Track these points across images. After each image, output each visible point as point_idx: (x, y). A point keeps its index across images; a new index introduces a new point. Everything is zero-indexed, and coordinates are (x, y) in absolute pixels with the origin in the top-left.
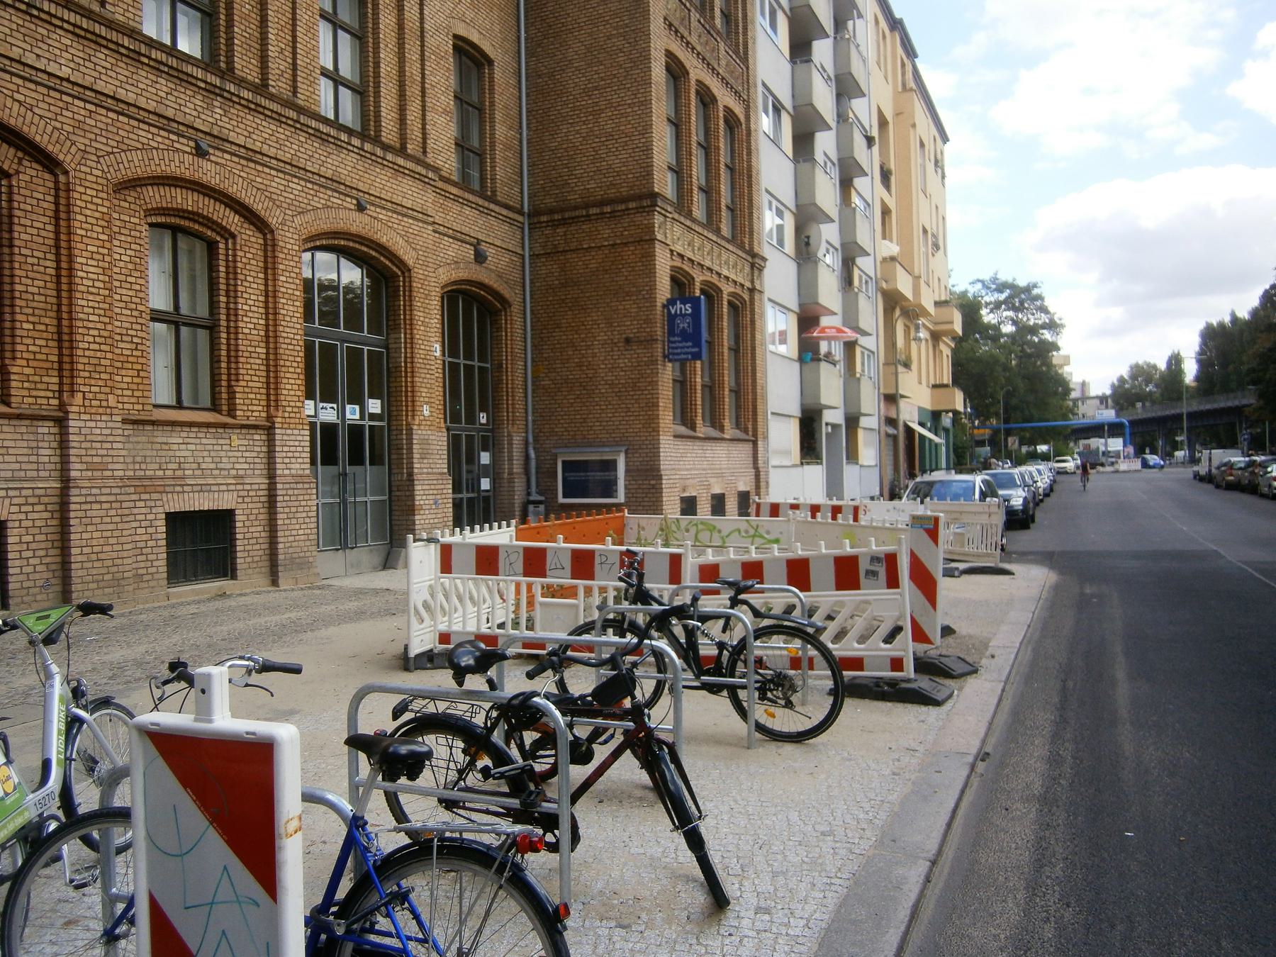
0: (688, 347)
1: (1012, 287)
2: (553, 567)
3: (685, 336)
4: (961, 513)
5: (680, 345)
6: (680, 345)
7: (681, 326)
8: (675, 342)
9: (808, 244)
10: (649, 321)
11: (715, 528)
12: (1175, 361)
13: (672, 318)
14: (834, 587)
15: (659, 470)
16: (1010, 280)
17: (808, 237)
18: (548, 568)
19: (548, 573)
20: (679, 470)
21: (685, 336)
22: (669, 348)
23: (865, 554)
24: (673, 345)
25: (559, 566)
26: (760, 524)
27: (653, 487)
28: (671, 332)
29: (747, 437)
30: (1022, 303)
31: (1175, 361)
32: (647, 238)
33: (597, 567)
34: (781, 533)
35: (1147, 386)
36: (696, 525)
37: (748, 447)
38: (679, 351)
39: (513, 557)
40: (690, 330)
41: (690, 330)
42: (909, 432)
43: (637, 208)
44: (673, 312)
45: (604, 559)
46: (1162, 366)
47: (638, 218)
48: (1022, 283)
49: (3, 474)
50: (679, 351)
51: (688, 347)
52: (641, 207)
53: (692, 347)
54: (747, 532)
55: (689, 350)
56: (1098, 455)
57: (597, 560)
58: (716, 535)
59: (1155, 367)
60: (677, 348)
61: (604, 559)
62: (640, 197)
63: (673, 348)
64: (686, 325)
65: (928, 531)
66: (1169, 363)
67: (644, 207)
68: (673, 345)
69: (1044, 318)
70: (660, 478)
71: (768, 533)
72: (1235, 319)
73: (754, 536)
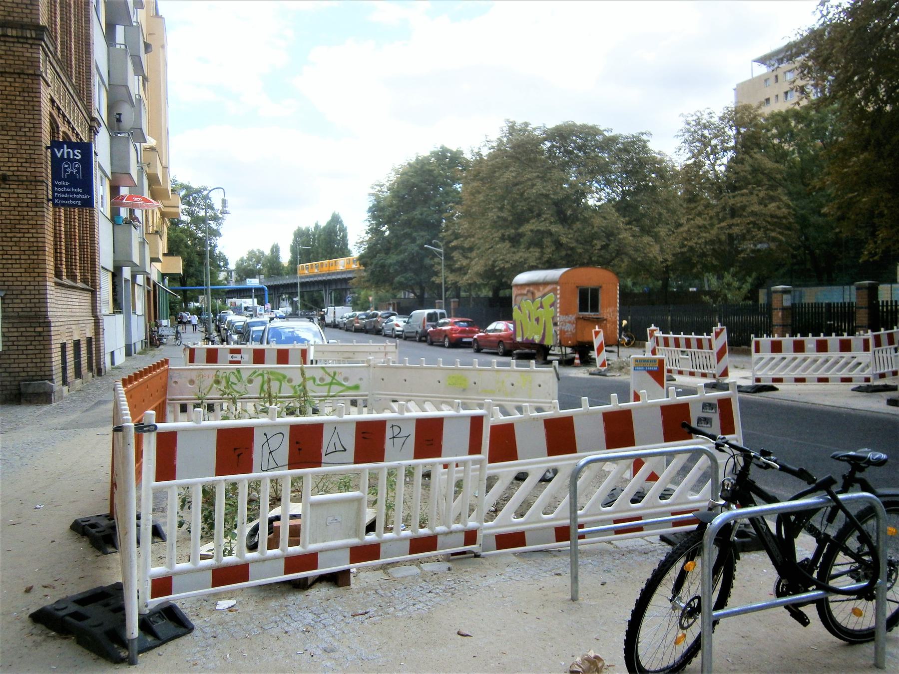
0: (77, 193)
1: (187, 188)
2: (331, 449)
3: (73, 181)
4: (354, 353)
5: (68, 190)
6: (68, 190)
7: (69, 170)
8: (61, 186)
9: (119, 120)
10: (30, 160)
11: (285, 377)
12: (275, 250)
13: (57, 163)
14: (663, 439)
15: (46, 317)
16: (185, 183)
17: (120, 115)
18: (324, 454)
19: (324, 459)
20: (60, 317)
21: (73, 181)
22: (53, 192)
23: (696, 401)
24: (60, 189)
25: (339, 447)
26: (337, 370)
27: (40, 334)
28: (56, 175)
29: (88, 287)
30: (194, 200)
31: (275, 250)
32: (31, 72)
33: (388, 443)
34: (361, 379)
35: (258, 265)
36: (262, 375)
37: (87, 296)
38: (66, 196)
39: (274, 443)
40: (80, 176)
41: (80, 176)
42: (155, 285)
43: (17, 37)
44: (59, 155)
45: (396, 430)
46: (268, 252)
47: (18, 48)
48: (195, 185)
49: (2, 159)
50: (66, 196)
51: (77, 193)
52: (22, 37)
53: (82, 194)
54: (322, 379)
55: (79, 196)
56: (241, 309)
57: (389, 433)
58: (285, 384)
59: (262, 253)
60: (64, 193)
61: (396, 430)
62: (23, 27)
63: (59, 192)
64: (75, 171)
65: (651, 372)
66: (272, 251)
67: (27, 38)
68: (60, 189)
69: (210, 213)
70: (48, 324)
71: (346, 379)
72: (317, 227)
73: (331, 384)
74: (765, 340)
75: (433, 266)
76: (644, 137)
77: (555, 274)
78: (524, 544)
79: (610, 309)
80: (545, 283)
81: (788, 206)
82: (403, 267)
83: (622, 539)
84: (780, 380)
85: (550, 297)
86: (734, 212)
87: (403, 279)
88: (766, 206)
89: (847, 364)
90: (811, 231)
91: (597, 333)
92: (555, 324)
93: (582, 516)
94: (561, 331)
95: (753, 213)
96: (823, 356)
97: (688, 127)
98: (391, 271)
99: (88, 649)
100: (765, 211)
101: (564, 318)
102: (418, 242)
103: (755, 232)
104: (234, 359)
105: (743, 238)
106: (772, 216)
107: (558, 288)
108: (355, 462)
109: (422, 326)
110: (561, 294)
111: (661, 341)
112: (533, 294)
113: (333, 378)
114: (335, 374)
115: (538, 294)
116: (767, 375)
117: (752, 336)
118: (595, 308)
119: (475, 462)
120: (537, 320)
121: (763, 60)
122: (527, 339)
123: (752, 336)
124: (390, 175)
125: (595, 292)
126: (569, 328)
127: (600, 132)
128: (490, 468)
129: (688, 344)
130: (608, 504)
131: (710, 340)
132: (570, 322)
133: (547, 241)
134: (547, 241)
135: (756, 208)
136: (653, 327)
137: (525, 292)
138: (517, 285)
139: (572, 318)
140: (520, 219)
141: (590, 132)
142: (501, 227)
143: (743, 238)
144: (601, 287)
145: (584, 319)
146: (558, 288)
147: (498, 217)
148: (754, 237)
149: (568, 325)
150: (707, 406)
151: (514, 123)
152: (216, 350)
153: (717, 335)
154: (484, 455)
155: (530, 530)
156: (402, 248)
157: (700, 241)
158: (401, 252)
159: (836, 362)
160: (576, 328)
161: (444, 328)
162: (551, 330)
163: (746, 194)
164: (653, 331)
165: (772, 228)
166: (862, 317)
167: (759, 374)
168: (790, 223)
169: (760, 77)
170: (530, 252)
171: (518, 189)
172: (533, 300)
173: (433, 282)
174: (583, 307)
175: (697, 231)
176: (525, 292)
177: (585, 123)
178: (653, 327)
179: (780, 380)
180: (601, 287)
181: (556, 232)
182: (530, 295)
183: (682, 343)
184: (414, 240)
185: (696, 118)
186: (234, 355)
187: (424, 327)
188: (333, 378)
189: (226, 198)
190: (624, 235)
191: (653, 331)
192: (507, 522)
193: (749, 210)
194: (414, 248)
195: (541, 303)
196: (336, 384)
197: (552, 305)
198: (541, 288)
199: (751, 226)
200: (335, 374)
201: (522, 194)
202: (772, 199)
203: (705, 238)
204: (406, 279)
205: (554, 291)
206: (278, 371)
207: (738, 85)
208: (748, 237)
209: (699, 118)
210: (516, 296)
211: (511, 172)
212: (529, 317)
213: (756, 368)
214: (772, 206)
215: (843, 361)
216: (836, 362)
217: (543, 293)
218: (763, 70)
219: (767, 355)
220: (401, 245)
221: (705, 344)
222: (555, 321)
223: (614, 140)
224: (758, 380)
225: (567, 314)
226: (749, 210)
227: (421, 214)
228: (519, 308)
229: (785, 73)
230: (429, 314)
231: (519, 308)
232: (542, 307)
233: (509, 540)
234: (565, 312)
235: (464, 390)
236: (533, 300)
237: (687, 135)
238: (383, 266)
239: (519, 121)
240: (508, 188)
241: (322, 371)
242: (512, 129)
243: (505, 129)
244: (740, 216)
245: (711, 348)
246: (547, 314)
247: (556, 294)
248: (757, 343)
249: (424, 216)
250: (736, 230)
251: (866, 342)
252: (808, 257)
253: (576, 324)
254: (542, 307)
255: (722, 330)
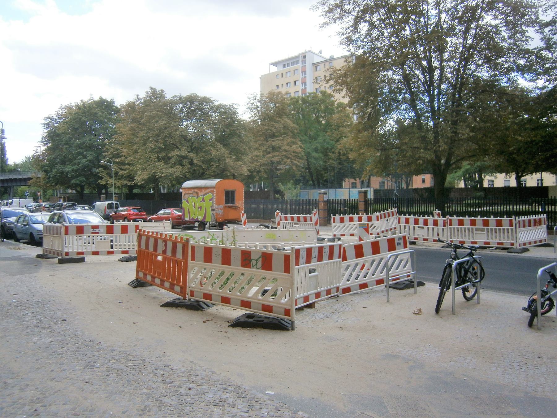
23: (396, 237)
65: (365, 229)
74: (337, 217)
75: (98, 173)
76: (235, 106)
77: (213, 182)
78: (350, 291)
79: (240, 202)
80: (206, 188)
81: (301, 147)
82: (78, 173)
83: (379, 287)
84: (343, 235)
85: (210, 195)
86: (274, 149)
87: (77, 182)
88: (291, 147)
89: (352, 227)
90: (313, 161)
91: (243, 215)
92: (213, 210)
93: (391, 274)
94: (216, 213)
95: (286, 151)
96: (343, 224)
97: (249, 100)
98: (69, 175)
99: (272, 329)
100: (290, 149)
101: (217, 207)
102: (88, 158)
103: (285, 160)
104: (95, 232)
105: (279, 163)
106: (294, 152)
107: (215, 190)
108: (318, 262)
109: (104, 212)
110: (216, 194)
111: (283, 218)
112: (197, 193)
113: (213, 237)
114: (213, 235)
115: (200, 194)
116: (338, 233)
117: (332, 215)
118: (233, 202)
119: (331, 263)
120: (200, 208)
121: (275, 64)
122: (193, 218)
123: (332, 215)
124: (59, 112)
125: (233, 192)
126: (220, 212)
127: (212, 102)
128: (343, 263)
129: (292, 219)
130: (348, 280)
131: (311, 217)
132: (220, 209)
133: (185, 162)
134: (185, 162)
135: (287, 147)
136: (278, 211)
137: (192, 192)
138: (185, 188)
139: (222, 206)
140: (168, 147)
141: (206, 100)
142: (157, 152)
143: (279, 163)
144: (236, 190)
145: (229, 207)
146: (215, 190)
147: (156, 146)
148: (285, 163)
149: (220, 210)
150: (400, 239)
151: (155, 90)
152: (127, 226)
153: (315, 214)
154: (341, 259)
155: (352, 286)
156: (77, 161)
157: (258, 164)
158: (75, 164)
159: (348, 227)
160: (224, 212)
161: (123, 213)
162: (210, 213)
163: (281, 140)
164: (278, 213)
165: (294, 158)
166: (361, 206)
167: (335, 233)
168: (303, 156)
169: (273, 73)
170: (176, 169)
171: (167, 131)
172: (198, 197)
173: (99, 184)
174: (227, 201)
175: (256, 158)
176: (192, 192)
177: (206, 96)
178: (278, 211)
179: (343, 235)
180: (236, 190)
181: (191, 157)
182: (195, 194)
183: (295, 219)
184: (85, 157)
185: (253, 96)
186: (95, 229)
187: (105, 212)
188: (213, 237)
189: (4, 128)
190: (228, 160)
191: (278, 213)
192: (361, 280)
193: (283, 148)
194: (85, 162)
195: (203, 198)
196: (214, 239)
197: (211, 200)
198: (203, 190)
199: (283, 157)
200: (213, 235)
201: (170, 134)
202: (294, 143)
203: (261, 162)
204: (80, 181)
205: (212, 192)
206: (190, 234)
207: (262, 76)
208: (283, 162)
209: (255, 96)
210: (185, 194)
211: (163, 120)
212: (195, 206)
213: (334, 230)
214: (294, 146)
215: (350, 226)
216: (348, 227)
217: (205, 193)
218: (274, 69)
219: (338, 224)
220: (76, 159)
221: (308, 219)
222: (213, 208)
223: (219, 107)
224: (335, 235)
225: (219, 205)
226: (283, 148)
227: (90, 140)
228: (187, 201)
229: (287, 73)
230: (108, 204)
231: (187, 201)
232: (203, 200)
233: (363, 286)
234: (218, 203)
235: (274, 240)
236: (198, 197)
237: (249, 104)
238: (62, 173)
239: (158, 88)
240: (161, 130)
241: (208, 233)
242: (154, 92)
243: (149, 93)
244: (278, 151)
245: (311, 221)
246: (207, 205)
247: (213, 194)
248: (334, 218)
249: (92, 142)
250: (276, 159)
251: (377, 217)
252: (308, 174)
253: (224, 210)
254: (203, 200)
255: (316, 212)
